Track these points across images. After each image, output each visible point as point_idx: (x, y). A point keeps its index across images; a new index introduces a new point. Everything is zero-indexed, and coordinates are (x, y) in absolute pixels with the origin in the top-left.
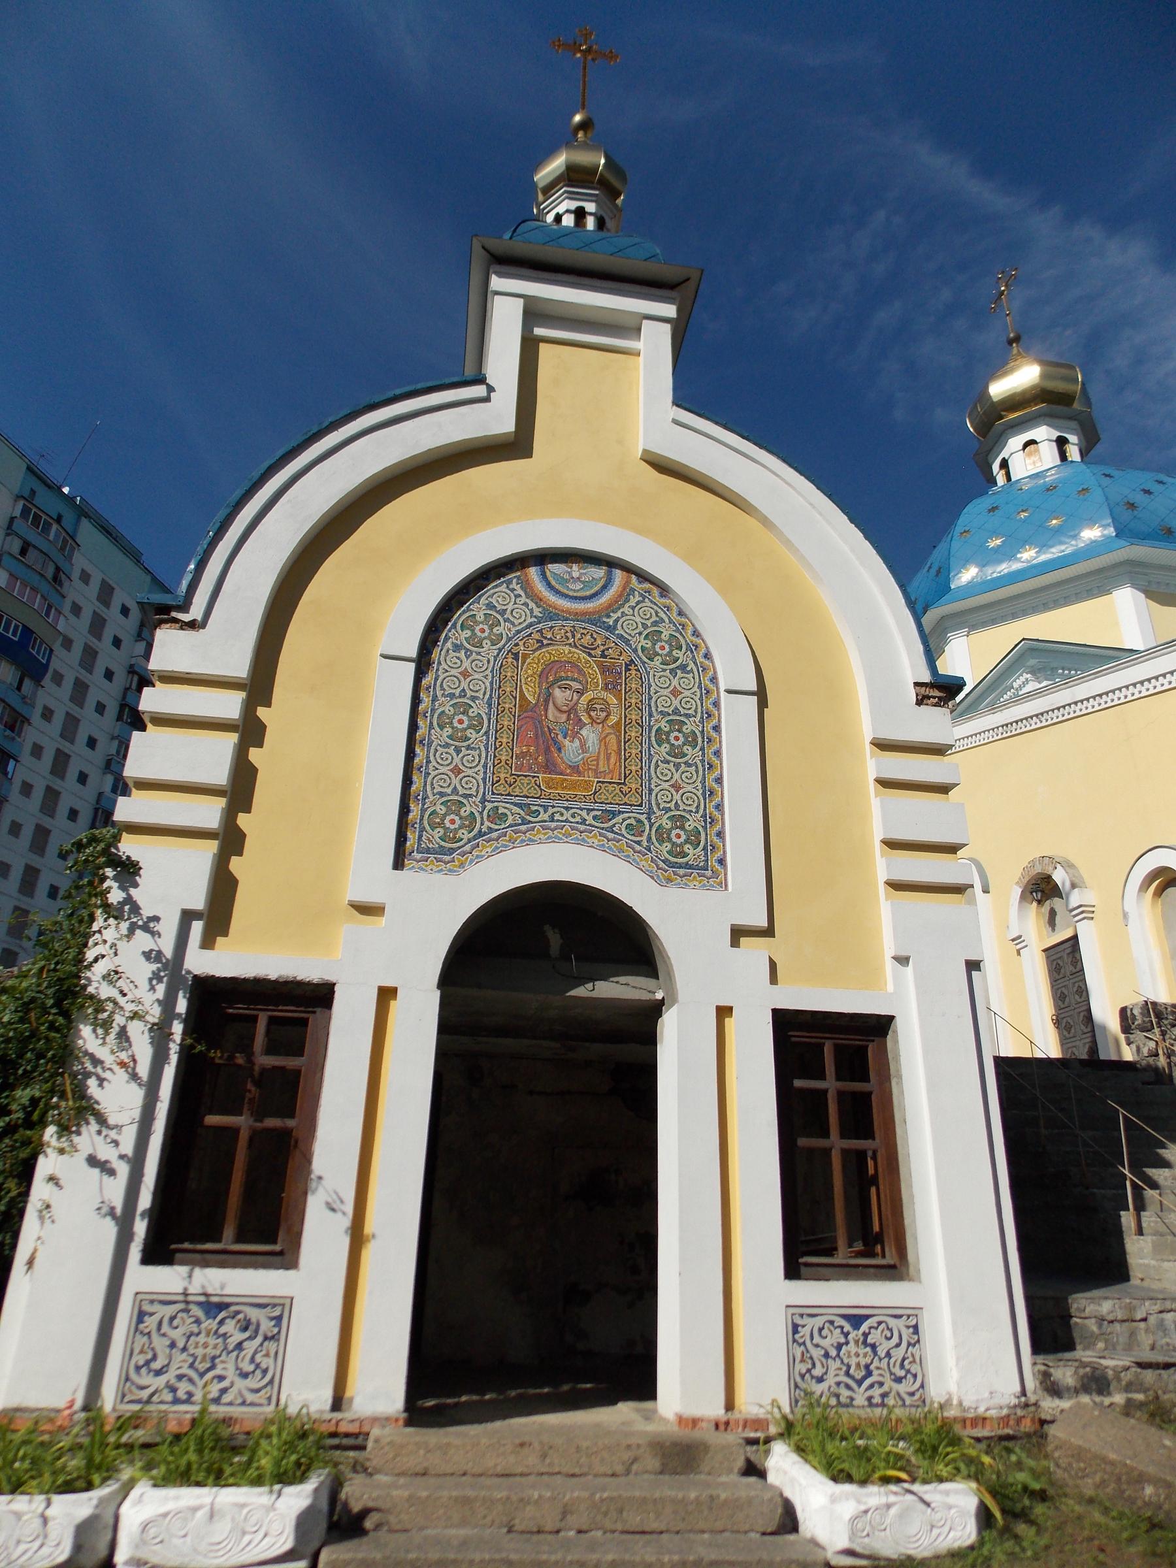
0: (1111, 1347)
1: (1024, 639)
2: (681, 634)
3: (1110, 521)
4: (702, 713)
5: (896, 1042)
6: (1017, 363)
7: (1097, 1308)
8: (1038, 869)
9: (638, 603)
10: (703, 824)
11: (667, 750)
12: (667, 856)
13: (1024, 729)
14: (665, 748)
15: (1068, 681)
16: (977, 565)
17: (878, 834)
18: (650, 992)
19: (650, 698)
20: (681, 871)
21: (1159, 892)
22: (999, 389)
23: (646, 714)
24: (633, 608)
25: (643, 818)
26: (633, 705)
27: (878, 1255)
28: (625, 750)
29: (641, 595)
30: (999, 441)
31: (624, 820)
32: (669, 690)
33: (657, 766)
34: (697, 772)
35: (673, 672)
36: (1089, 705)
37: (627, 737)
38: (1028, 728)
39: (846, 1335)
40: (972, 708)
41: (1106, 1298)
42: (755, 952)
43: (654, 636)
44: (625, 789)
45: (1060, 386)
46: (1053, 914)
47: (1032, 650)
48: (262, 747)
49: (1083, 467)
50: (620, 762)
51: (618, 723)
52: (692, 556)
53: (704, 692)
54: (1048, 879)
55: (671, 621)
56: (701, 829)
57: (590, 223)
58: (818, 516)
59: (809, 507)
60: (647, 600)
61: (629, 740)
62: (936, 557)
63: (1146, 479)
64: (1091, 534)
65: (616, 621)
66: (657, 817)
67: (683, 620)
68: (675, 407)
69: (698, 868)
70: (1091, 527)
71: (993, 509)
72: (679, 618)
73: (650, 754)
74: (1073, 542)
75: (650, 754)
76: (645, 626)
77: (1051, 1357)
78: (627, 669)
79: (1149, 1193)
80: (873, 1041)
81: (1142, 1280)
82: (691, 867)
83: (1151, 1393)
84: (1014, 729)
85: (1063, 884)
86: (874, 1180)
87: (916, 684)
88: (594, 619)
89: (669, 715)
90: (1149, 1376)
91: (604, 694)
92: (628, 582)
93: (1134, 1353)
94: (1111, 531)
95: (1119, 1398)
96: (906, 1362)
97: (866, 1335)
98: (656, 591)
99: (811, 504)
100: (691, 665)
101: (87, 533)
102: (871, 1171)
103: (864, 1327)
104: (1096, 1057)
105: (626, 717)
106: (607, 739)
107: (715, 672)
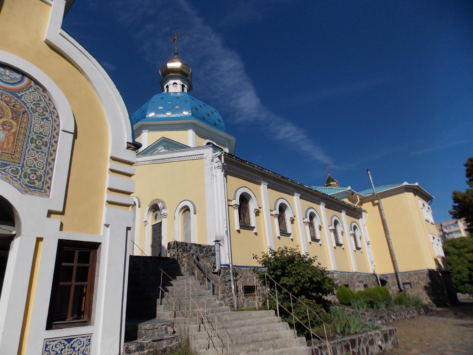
0: (147, 337)
1: (163, 137)
2: (48, 107)
3: (191, 111)
4: (51, 136)
5: (100, 251)
6: (176, 60)
7: (146, 326)
8: (155, 202)
9: (33, 91)
10: (44, 174)
11: (34, 146)
12: (27, 183)
13: (158, 162)
14: (34, 145)
15: (172, 151)
16: (154, 113)
17: (107, 186)
18: (10, 231)
19: (31, 126)
20: (32, 189)
21: (184, 212)
22: (170, 65)
23: (28, 132)
24: (30, 93)
25: (19, 168)
26: (23, 127)
27: (82, 318)
28: (16, 142)
29: (34, 89)
30: (167, 80)
31: (11, 168)
32: (40, 125)
33: (29, 151)
34: (45, 156)
35: (43, 119)
36: (173, 160)
37: (18, 138)
38: (160, 162)
39: (65, 346)
40: (146, 152)
41: (148, 324)
42: (56, 220)
43: (38, 105)
44: (13, 156)
45: (185, 71)
46: (156, 215)
47: (165, 141)
49: (187, 95)
50: (13, 147)
51: (15, 133)
52: (58, 81)
53: (54, 129)
54: (157, 205)
55: (45, 101)
56: (43, 176)
58: (106, 83)
59: (104, 79)
60: (37, 91)
61: (19, 139)
62: (144, 107)
63: (201, 103)
64: (185, 113)
65: (22, 95)
66: (25, 169)
67: (50, 102)
68: (61, 29)
69: (39, 189)
70: (186, 112)
71: (162, 98)
72: (49, 101)
73: (27, 146)
74: (181, 114)
75: (27, 146)
76: (34, 100)
77: (130, 342)
78: (23, 114)
79: (166, 293)
80: (93, 250)
81: (159, 317)
82: (36, 188)
83: (155, 348)
84: (156, 162)
85: (161, 207)
86: (85, 295)
87: (128, 143)
88: (13, 92)
89: (38, 134)
90: (155, 343)
91: (11, 121)
92: (30, 83)
93: (153, 338)
94: (190, 114)
95: (146, 351)
96: (84, 351)
97: (72, 345)
98: (41, 89)
99: (105, 78)
100: (50, 119)
102: (84, 292)
103: (72, 342)
104: (160, 256)
105: (19, 131)
106: (9, 137)
107: (59, 123)
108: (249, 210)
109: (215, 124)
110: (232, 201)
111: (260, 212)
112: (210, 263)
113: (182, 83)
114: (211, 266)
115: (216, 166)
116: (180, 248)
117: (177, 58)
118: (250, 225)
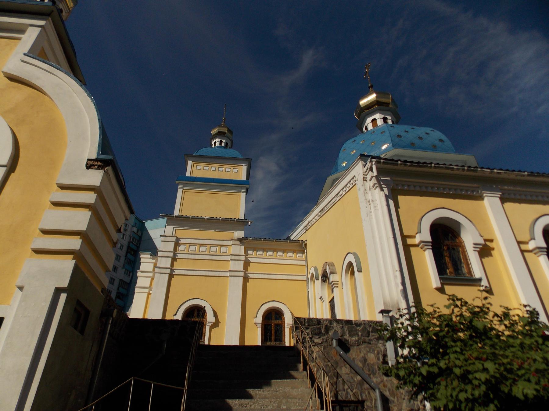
57: (390, 122)
109: (435, 146)
110: (415, 237)
111: (493, 249)
112: (374, 354)
113: (382, 116)
114: (379, 359)
115: (372, 185)
116: (307, 328)
117: (372, 91)
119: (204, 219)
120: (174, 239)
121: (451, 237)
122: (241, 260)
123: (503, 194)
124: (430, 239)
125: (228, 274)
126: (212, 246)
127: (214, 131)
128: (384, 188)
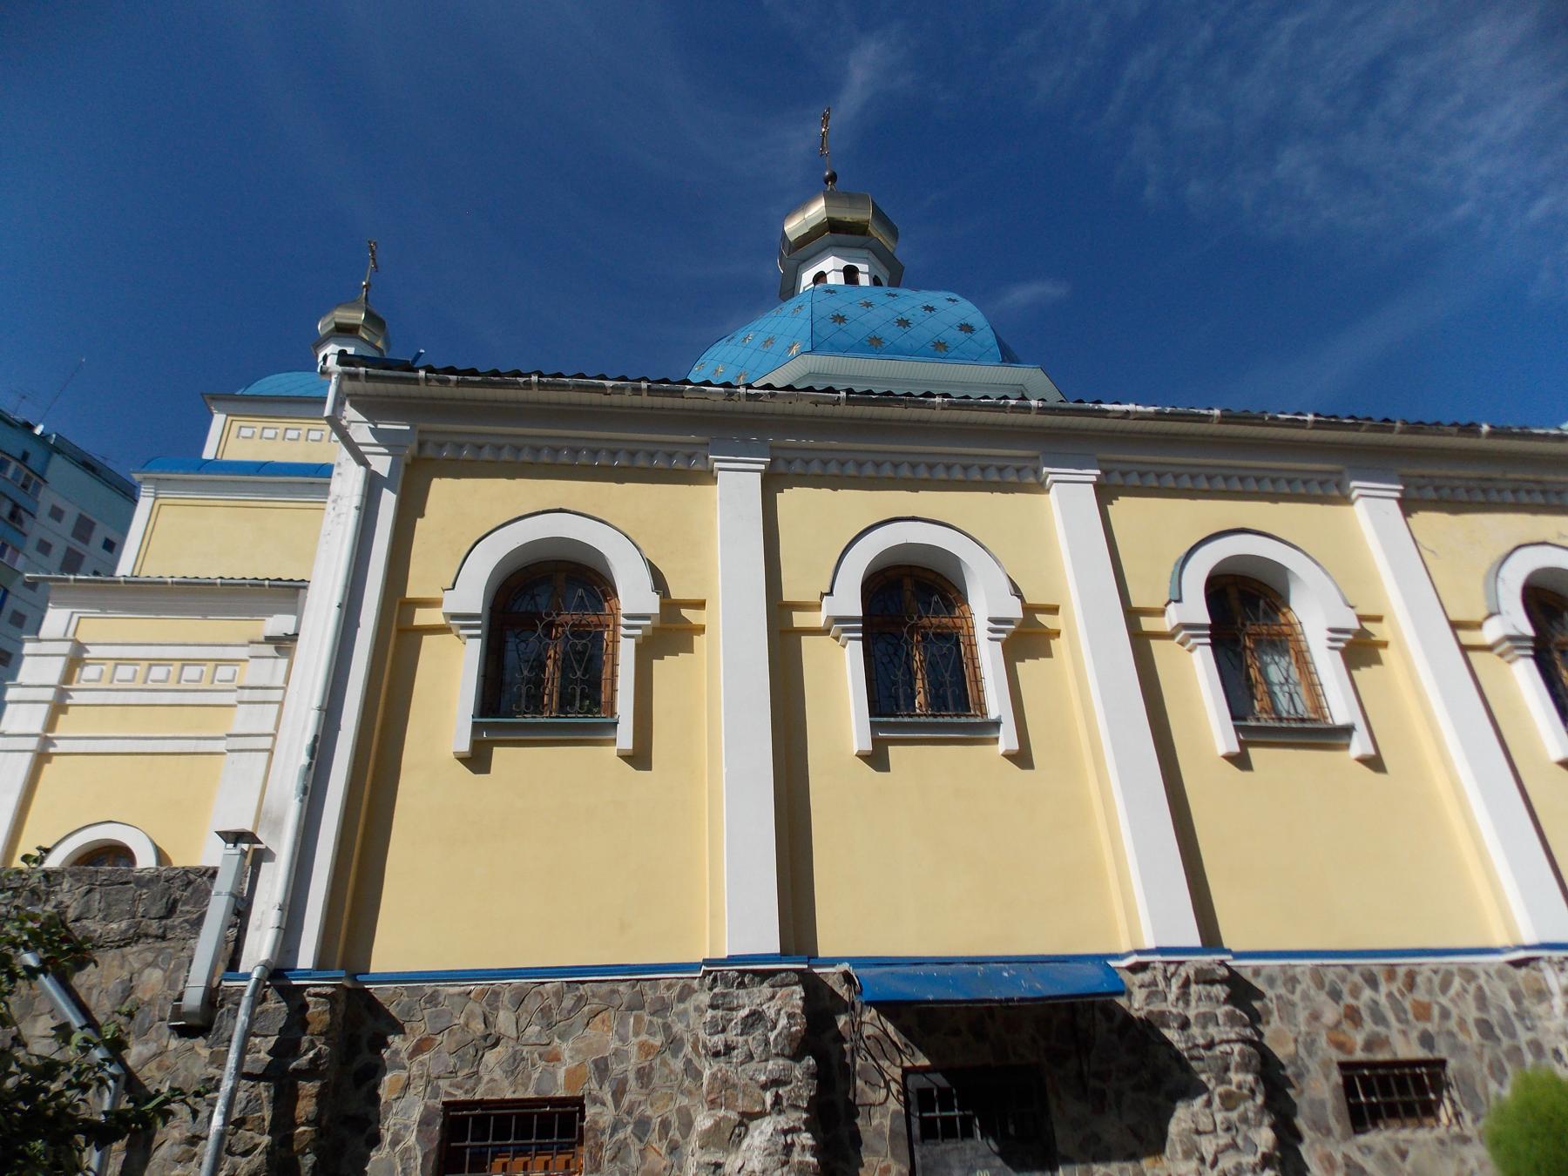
48: (651, 770)
57: (864, 280)
101: (59, 468)
108: (1298, 641)
110: (1162, 613)
118: (1325, 718)
119: (215, 584)
120: (66, 648)
121: (1265, 613)
122: (270, 702)
123: (1106, 473)
124: (1205, 619)
125: (221, 746)
126: (221, 665)
127: (323, 327)
128: (366, 456)
